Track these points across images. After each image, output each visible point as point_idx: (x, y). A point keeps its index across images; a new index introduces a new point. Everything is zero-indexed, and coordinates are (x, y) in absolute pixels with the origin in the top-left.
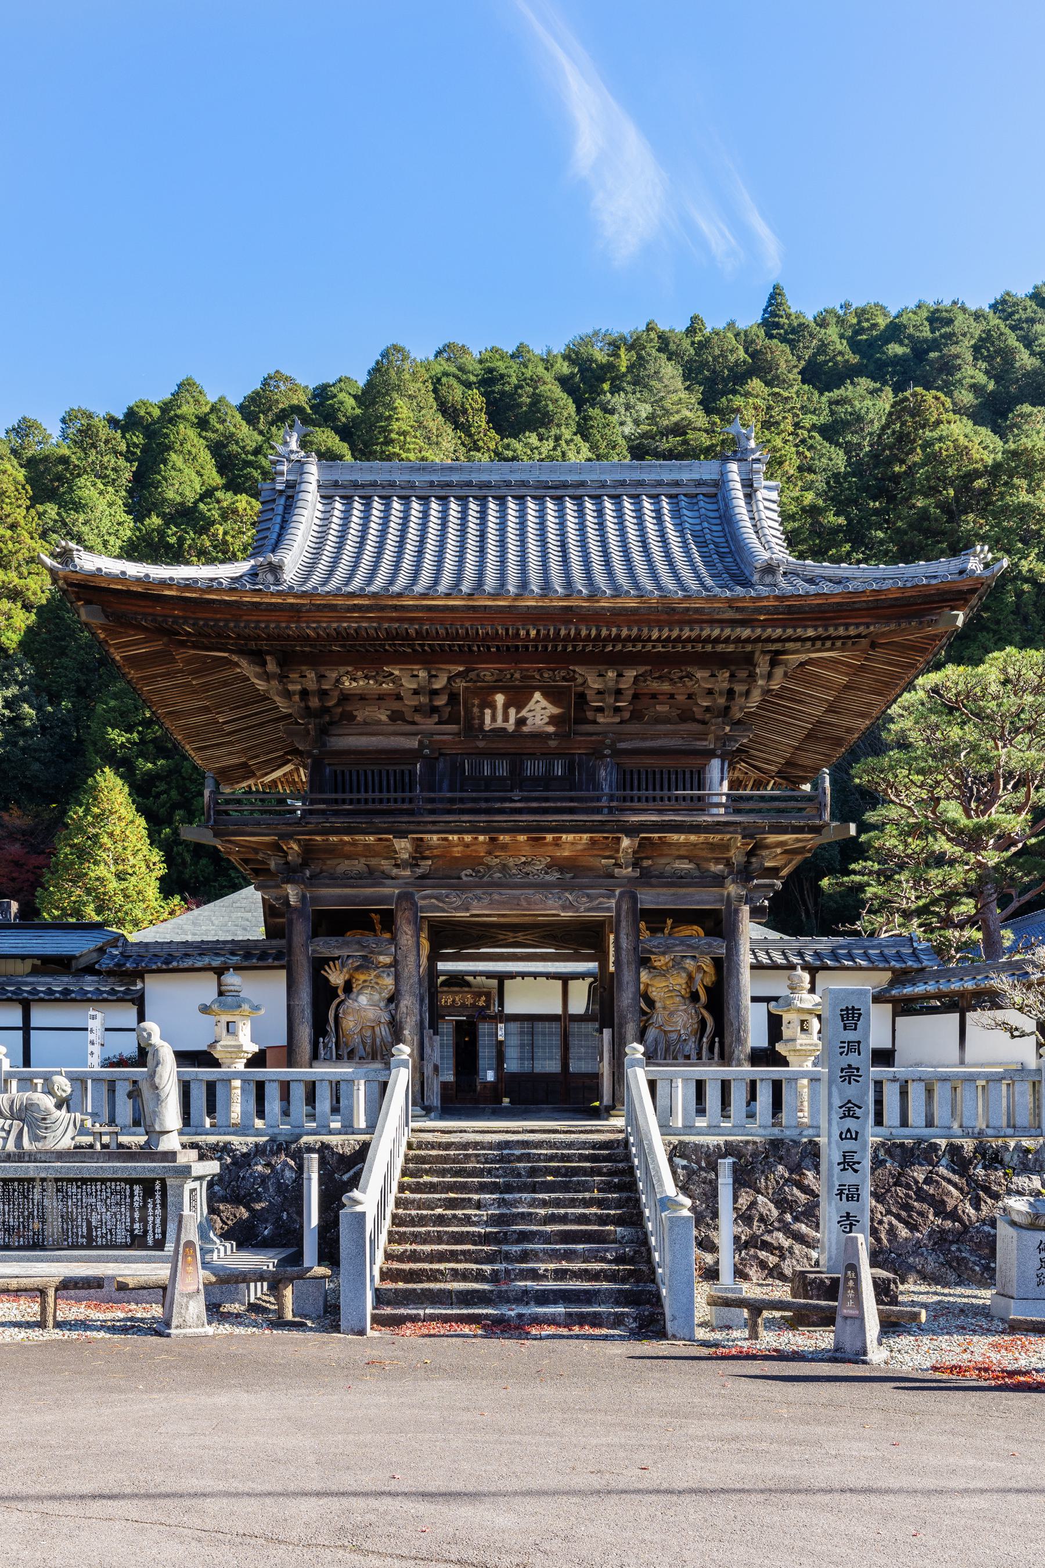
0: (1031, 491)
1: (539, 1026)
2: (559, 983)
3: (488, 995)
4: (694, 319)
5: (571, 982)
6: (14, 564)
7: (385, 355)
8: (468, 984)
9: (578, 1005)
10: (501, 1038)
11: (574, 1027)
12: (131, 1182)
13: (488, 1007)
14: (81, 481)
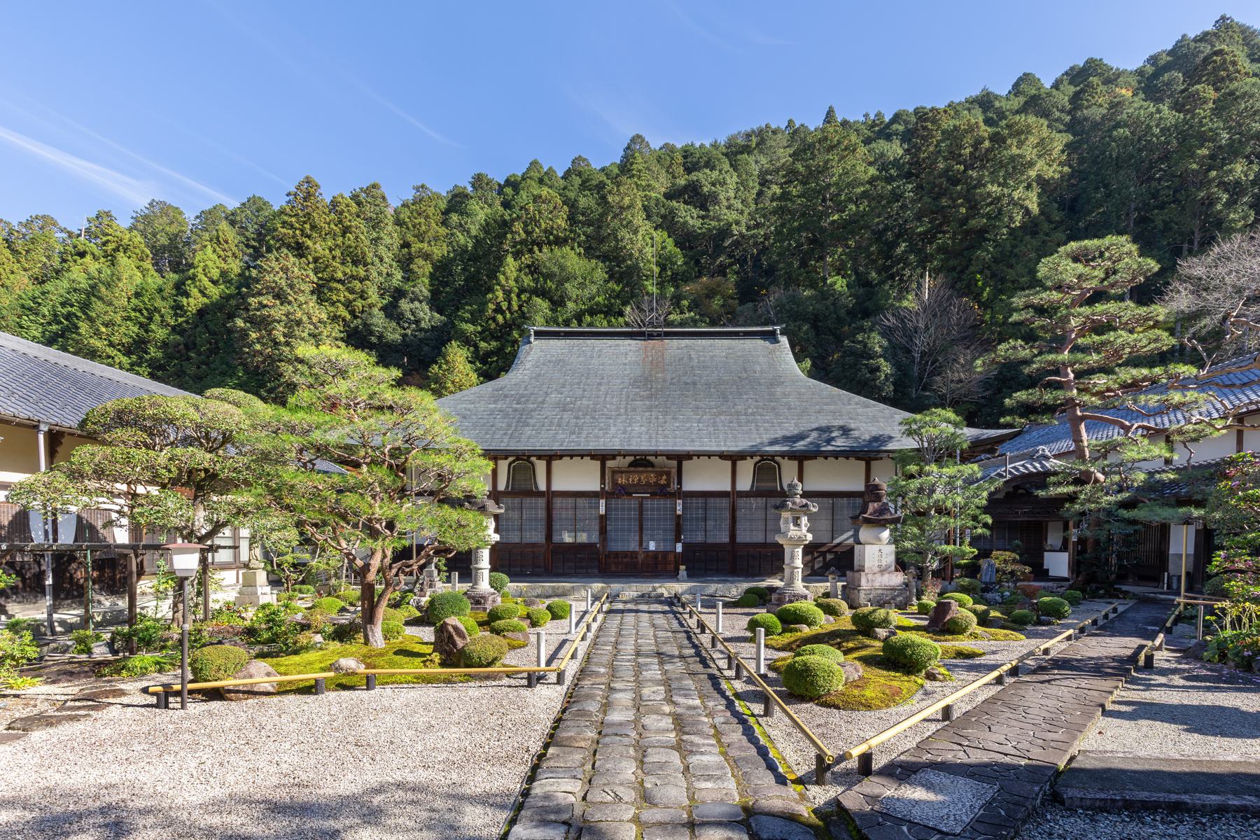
0: (1018, 147)
1: (712, 500)
2: (729, 463)
3: (668, 474)
4: (790, 121)
5: (806, 463)
6: (427, 239)
7: (633, 140)
8: (651, 465)
9: (745, 484)
10: (679, 513)
11: (741, 502)
13: (668, 485)
14: (472, 201)
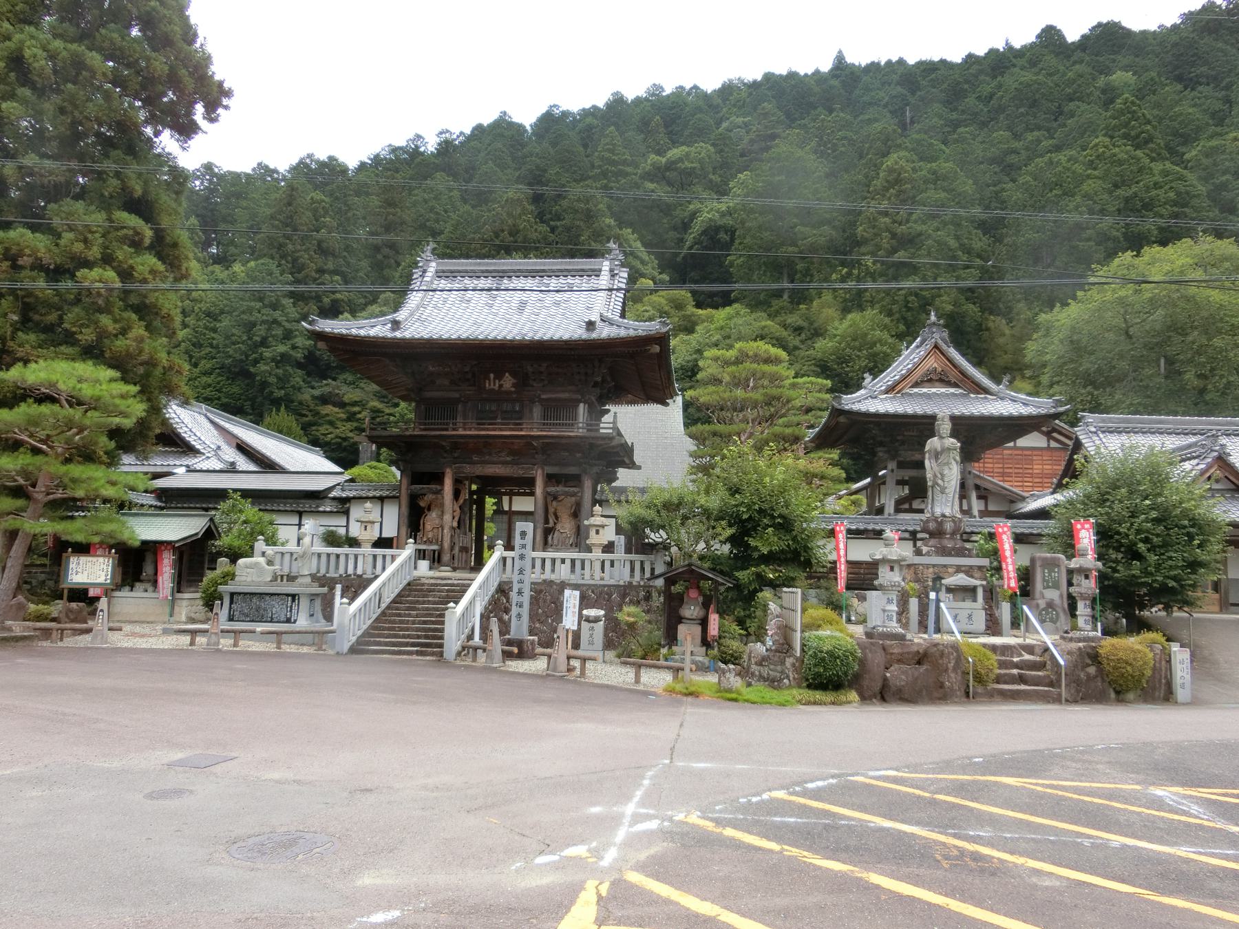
12: (288, 595)
